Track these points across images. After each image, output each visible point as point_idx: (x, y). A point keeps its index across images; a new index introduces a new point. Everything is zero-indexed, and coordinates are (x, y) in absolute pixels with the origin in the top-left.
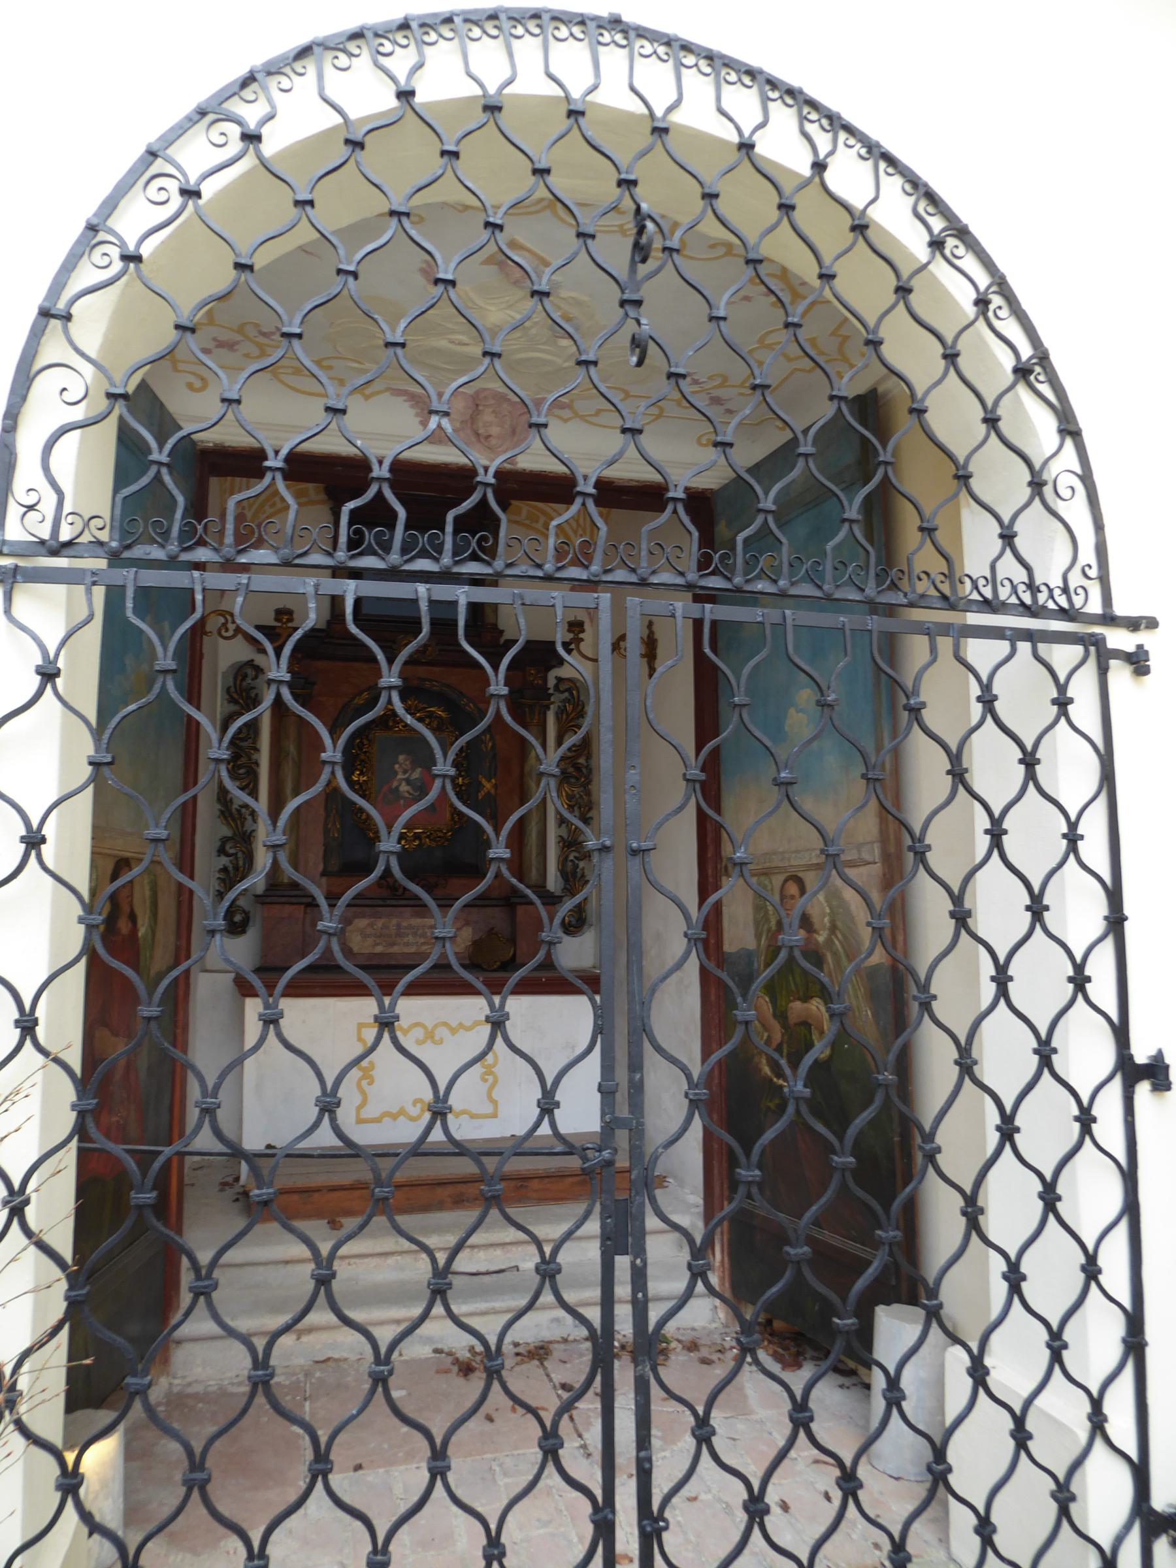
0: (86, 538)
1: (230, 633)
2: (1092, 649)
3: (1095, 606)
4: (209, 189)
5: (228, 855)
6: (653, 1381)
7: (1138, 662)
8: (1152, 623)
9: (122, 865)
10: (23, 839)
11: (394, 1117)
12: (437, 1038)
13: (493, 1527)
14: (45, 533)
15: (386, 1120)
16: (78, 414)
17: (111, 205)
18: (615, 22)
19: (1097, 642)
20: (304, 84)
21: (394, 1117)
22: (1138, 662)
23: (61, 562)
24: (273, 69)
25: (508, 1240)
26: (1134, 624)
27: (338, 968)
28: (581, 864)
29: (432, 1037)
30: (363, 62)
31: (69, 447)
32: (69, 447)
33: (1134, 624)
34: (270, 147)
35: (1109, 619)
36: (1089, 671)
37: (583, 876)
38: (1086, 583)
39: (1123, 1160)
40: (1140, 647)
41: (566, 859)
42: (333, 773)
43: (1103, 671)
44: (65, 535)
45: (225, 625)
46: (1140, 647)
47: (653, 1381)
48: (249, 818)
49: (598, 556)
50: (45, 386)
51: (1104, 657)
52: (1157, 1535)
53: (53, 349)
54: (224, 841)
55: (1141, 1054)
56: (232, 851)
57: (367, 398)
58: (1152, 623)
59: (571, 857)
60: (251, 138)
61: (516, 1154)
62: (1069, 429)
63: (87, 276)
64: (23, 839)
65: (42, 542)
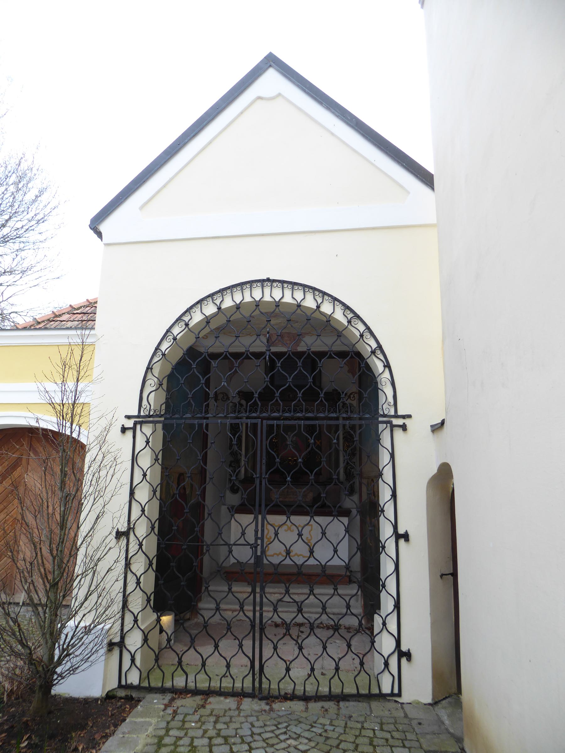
0: (155, 414)
1: (225, 399)
2: (388, 425)
3: (392, 413)
4: (178, 337)
5: (232, 467)
6: (264, 596)
7: (404, 427)
8: (409, 416)
9: (181, 477)
10: (143, 475)
11: (278, 555)
12: (292, 529)
13: (287, 674)
14: (147, 414)
15: (275, 556)
16: (154, 388)
17: (160, 344)
18: (268, 280)
19: (390, 422)
20: (197, 310)
21: (278, 555)
22: (404, 427)
23: (151, 419)
24: (191, 308)
25: (299, 592)
26: (404, 417)
27: (246, 505)
28: (352, 470)
29: (290, 529)
30: (210, 302)
31: (153, 394)
32: (153, 394)
33: (404, 417)
34: (190, 326)
35: (396, 416)
36: (388, 431)
37: (353, 474)
38: (389, 407)
39: (395, 559)
40: (404, 423)
41: (347, 468)
42: (200, 462)
43: (392, 431)
44: (152, 413)
45: (223, 397)
46: (404, 423)
47: (264, 596)
48: (239, 455)
49: (259, 411)
50: (148, 383)
51: (393, 427)
52: (403, 656)
53: (149, 376)
54: (231, 462)
55: (401, 531)
56: (234, 466)
57: (251, 336)
58: (409, 416)
59: (349, 468)
60: (187, 325)
61: (234, 545)
62: (387, 366)
63: (156, 359)
64: (143, 475)
65: (147, 415)
